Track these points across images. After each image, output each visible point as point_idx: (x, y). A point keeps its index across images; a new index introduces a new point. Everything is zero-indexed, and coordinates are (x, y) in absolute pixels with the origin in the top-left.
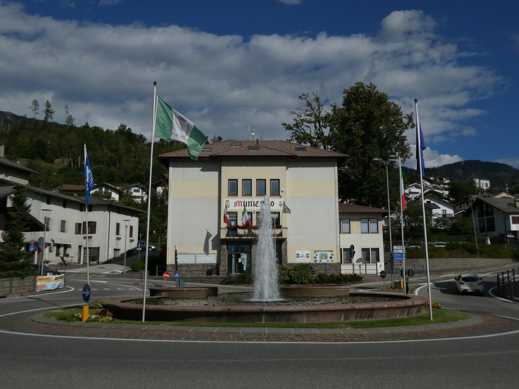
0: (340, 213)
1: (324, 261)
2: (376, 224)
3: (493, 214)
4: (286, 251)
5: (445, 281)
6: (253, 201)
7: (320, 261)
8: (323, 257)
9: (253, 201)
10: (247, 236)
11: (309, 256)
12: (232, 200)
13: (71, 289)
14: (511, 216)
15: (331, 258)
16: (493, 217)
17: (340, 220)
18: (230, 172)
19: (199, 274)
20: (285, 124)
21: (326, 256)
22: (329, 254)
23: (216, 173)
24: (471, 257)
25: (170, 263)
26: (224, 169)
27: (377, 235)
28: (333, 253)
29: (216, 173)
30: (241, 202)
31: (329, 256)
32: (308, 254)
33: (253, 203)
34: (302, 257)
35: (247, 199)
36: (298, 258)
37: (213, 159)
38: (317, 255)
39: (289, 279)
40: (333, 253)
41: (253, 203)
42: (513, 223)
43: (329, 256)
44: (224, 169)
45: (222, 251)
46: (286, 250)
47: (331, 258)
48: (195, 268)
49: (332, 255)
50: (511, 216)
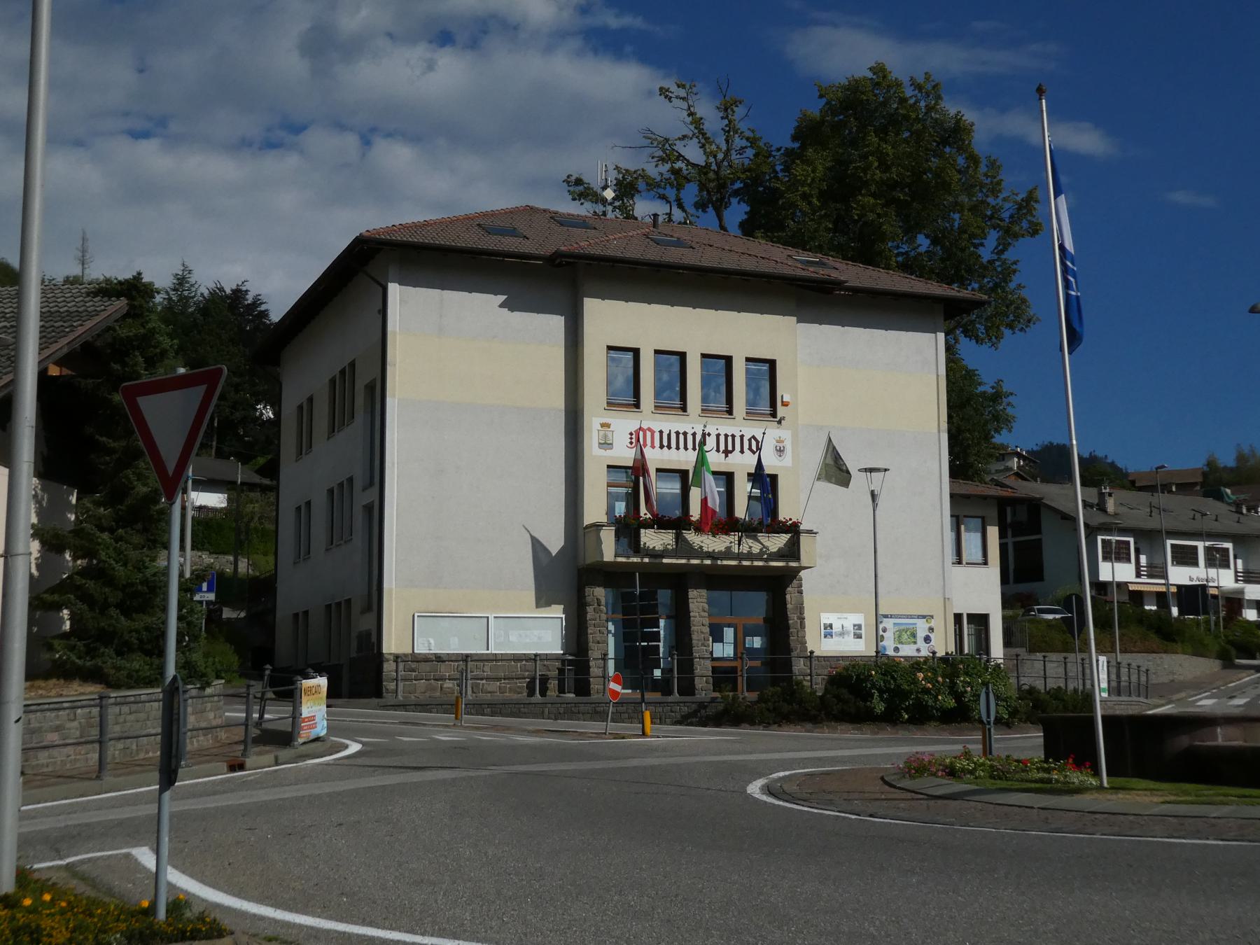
0: (952, 496)
1: (908, 651)
2: (978, 536)
3: (1039, 532)
4: (802, 612)
5: (725, 758)
6: (690, 432)
7: (897, 649)
8: (905, 636)
9: (690, 432)
10: (674, 554)
11: (863, 632)
12: (624, 424)
13: (346, 747)
14: (1169, 542)
15: (927, 639)
16: (1040, 540)
17: (957, 522)
18: (611, 320)
19: (502, 690)
20: (579, 182)
21: (914, 635)
22: (922, 628)
23: (556, 323)
24: (1165, 652)
25: (394, 650)
26: (592, 307)
27: (982, 570)
28: (933, 623)
29: (556, 323)
30: (653, 432)
31: (921, 635)
32: (859, 627)
33: (690, 438)
34: (842, 634)
35: (719, 427)
36: (829, 640)
37: (560, 265)
38: (931, 629)
39: (952, 703)
40: (933, 623)
41: (690, 438)
42: (1105, 559)
43: (921, 635)
44: (592, 307)
45: (590, 609)
46: (800, 609)
47: (927, 639)
48: (487, 670)
49: (931, 629)
50: (1169, 542)
